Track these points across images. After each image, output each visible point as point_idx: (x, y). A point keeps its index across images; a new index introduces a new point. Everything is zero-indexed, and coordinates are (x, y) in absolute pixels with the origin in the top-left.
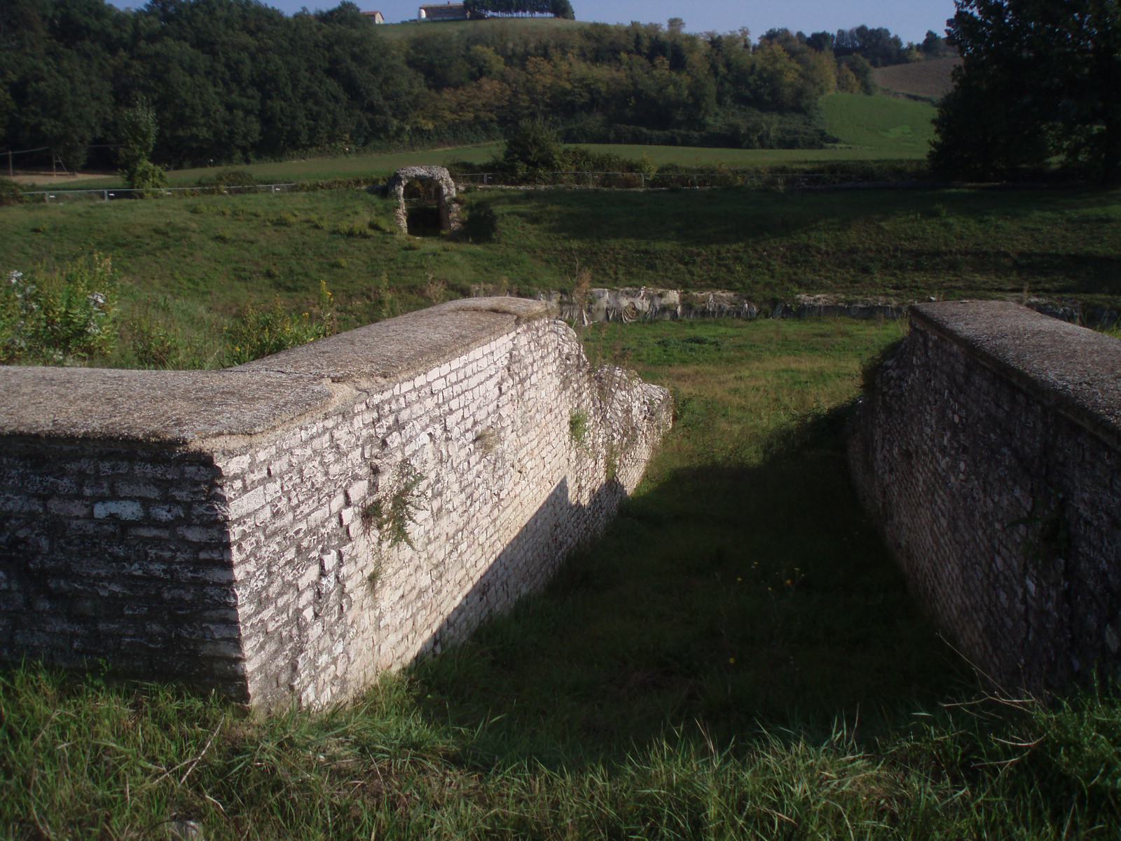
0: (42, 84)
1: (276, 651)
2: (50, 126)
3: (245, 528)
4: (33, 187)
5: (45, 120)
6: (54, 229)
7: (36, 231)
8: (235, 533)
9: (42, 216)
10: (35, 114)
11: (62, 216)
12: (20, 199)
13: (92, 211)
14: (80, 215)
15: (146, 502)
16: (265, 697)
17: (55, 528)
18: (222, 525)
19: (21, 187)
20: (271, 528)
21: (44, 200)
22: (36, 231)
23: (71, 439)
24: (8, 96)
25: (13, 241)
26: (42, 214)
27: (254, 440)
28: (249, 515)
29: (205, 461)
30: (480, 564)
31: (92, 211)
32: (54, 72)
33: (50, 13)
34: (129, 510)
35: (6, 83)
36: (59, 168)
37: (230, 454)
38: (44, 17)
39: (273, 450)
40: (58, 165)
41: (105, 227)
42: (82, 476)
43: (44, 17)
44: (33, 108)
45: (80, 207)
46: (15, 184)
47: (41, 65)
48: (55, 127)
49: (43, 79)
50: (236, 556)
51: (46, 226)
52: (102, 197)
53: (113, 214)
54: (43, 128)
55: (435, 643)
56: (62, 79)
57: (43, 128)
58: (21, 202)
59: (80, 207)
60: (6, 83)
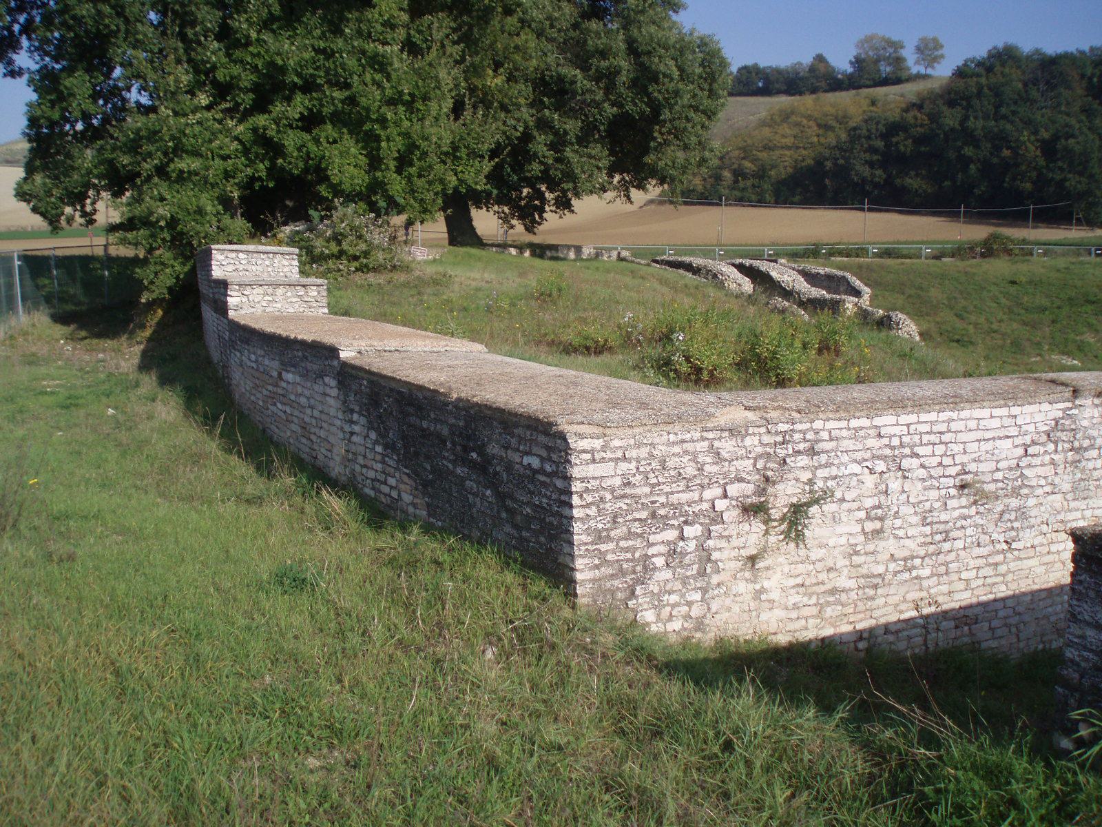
0: (1071, 141)
1: (613, 575)
2: (1074, 182)
3: (589, 486)
4: (1024, 241)
5: (1070, 176)
6: (1030, 282)
7: (1013, 282)
8: (576, 487)
9: (1023, 269)
10: (1061, 169)
11: (1042, 270)
12: (1009, 252)
13: (1072, 267)
14: (1058, 271)
15: (542, 459)
16: (595, 601)
17: (509, 467)
18: (568, 479)
19: (1012, 241)
20: (619, 492)
21: (1031, 254)
22: (1013, 282)
23: (516, 415)
24: (1038, 153)
25: (989, 291)
26: (1023, 267)
27: (608, 431)
28: (594, 478)
29: (562, 437)
30: (957, 596)
31: (1072, 267)
32: (1085, 130)
33: (1089, 71)
34: (535, 462)
35: (1037, 140)
36: (1079, 222)
37: (581, 436)
38: (1083, 76)
39: (632, 442)
40: (1078, 220)
41: (1079, 283)
42: (521, 440)
43: (1083, 76)
44: (1060, 164)
45: (1061, 262)
46: (1008, 238)
47: (1073, 121)
48: (1080, 182)
49: (1073, 136)
50: (575, 500)
51: (1024, 279)
52: (1090, 254)
53: (1091, 271)
54: (1067, 184)
55: (861, 638)
56: (1091, 137)
57: (1067, 184)
58: (1010, 255)
59: (1061, 262)
60: (1037, 140)
